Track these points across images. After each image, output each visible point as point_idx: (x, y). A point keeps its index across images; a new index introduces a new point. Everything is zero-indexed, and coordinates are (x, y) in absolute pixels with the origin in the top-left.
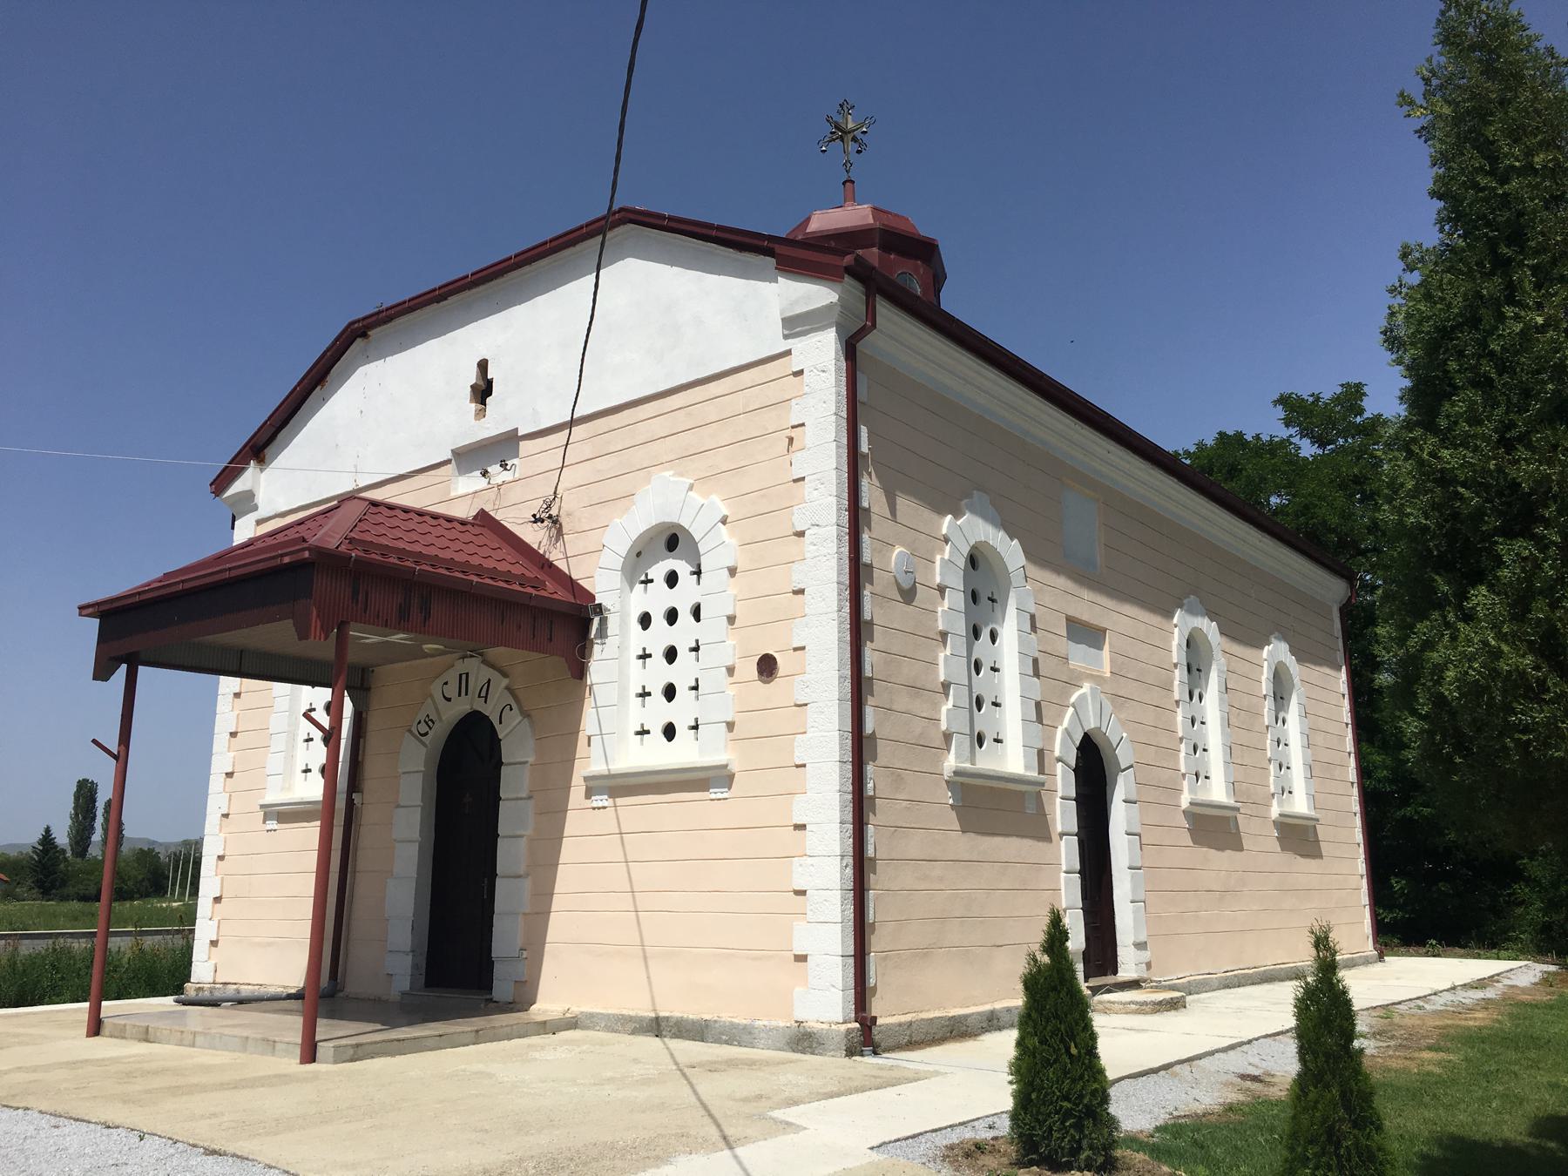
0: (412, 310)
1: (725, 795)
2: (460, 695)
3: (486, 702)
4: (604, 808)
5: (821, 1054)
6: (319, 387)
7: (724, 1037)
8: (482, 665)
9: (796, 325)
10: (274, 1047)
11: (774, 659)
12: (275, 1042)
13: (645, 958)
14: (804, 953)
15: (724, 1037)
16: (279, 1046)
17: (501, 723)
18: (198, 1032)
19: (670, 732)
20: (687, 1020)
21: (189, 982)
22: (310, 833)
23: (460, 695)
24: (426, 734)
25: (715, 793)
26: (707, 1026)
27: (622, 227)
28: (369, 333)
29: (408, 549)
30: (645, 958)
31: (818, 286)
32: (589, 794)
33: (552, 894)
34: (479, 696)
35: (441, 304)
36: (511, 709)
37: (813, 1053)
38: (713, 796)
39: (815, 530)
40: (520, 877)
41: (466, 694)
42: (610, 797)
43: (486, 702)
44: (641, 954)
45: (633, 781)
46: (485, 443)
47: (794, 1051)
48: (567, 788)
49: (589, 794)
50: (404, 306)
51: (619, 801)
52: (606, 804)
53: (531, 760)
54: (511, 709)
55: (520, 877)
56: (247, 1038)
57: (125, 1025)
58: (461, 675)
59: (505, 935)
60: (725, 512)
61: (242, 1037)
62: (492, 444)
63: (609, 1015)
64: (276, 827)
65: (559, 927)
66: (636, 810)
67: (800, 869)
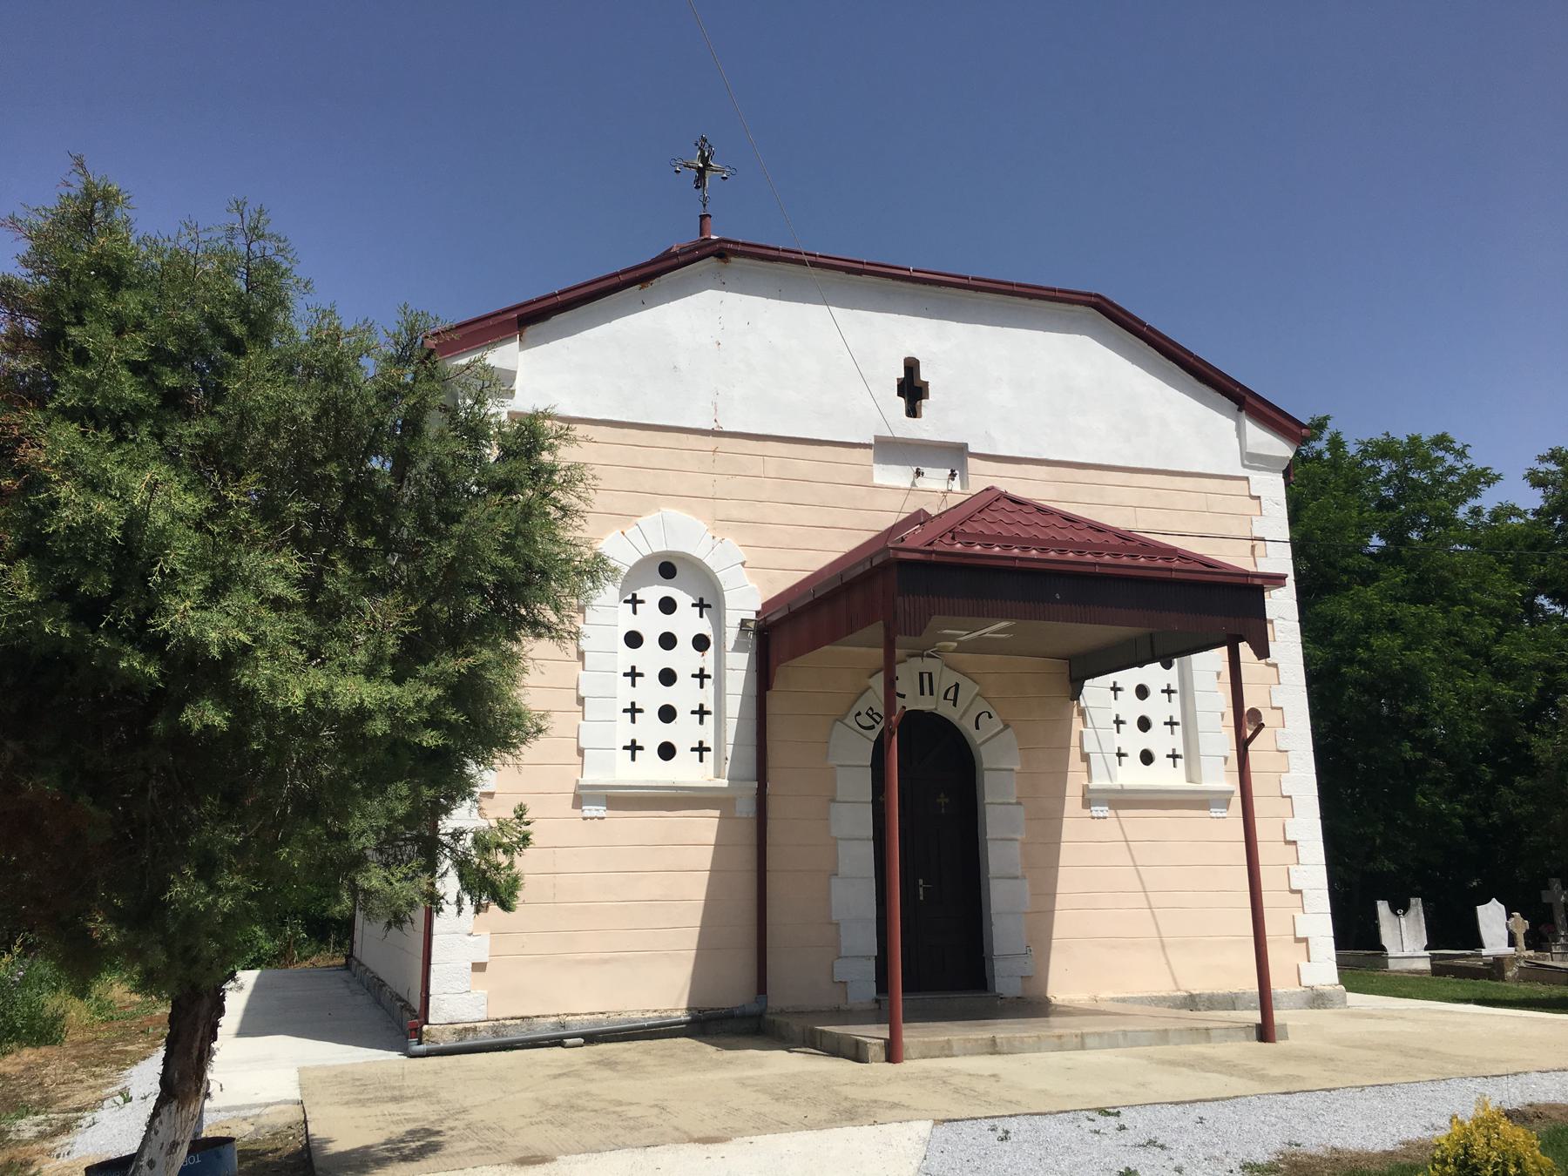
0: (1031, 297)
1: (1224, 815)
2: (922, 693)
3: (955, 705)
4: (1105, 818)
5: (1331, 1008)
6: (638, 286)
7: (1252, 1005)
8: (945, 668)
9: (1253, 460)
10: (1208, 1034)
11: (1260, 713)
12: (1207, 1029)
13: (1163, 947)
14: (1305, 936)
15: (1252, 1005)
16: (1212, 1033)
17: (977, 728)
18: (1088, 1034)
19: (1147, 757)
20: (1218, 995)
21: (427, 1023)
22: (704, 826)
23: (922, 693)
24: (872, 727)
25: (1215, 812)
26: (1237, 997)
27: (1083, 306)
28: (732, 259)
29: (1004, 534)
30: (1163, 947)
31: (1279, 441)
32: (1087, 803)
33: (1054, 895)
34: (945, 698)
35: (850, 276)
36: (990, 717)
37: (1325, 1008)
38: (1213, 815)
39: (1281, 621)
40: (1016, 878)
41: (931, 694)
42: (1110, 809)
43: (955, 705)
44: (1159, 944)
45: (1167, 797)
46: (910, 442)
47: (1311, 1008)
48: (1061, 797)
49: (1087, 803)
50: (799, 256)
51: (1121, 813)
52: (1107, 815)
53: (1017, 767)
54: (990, 717)
55: (1016, 878)
56: (1166, 1031)
57: (948, 1042)
58: (921, 675)
59: (1003, 931)
60: (744, 558)
61: (1158, 1031)
62: (901, 443)
63: (1142, 997)
64: (604, 815)
65: (1064, 923)
66: (1138, 822)
67: (1295, 874)
